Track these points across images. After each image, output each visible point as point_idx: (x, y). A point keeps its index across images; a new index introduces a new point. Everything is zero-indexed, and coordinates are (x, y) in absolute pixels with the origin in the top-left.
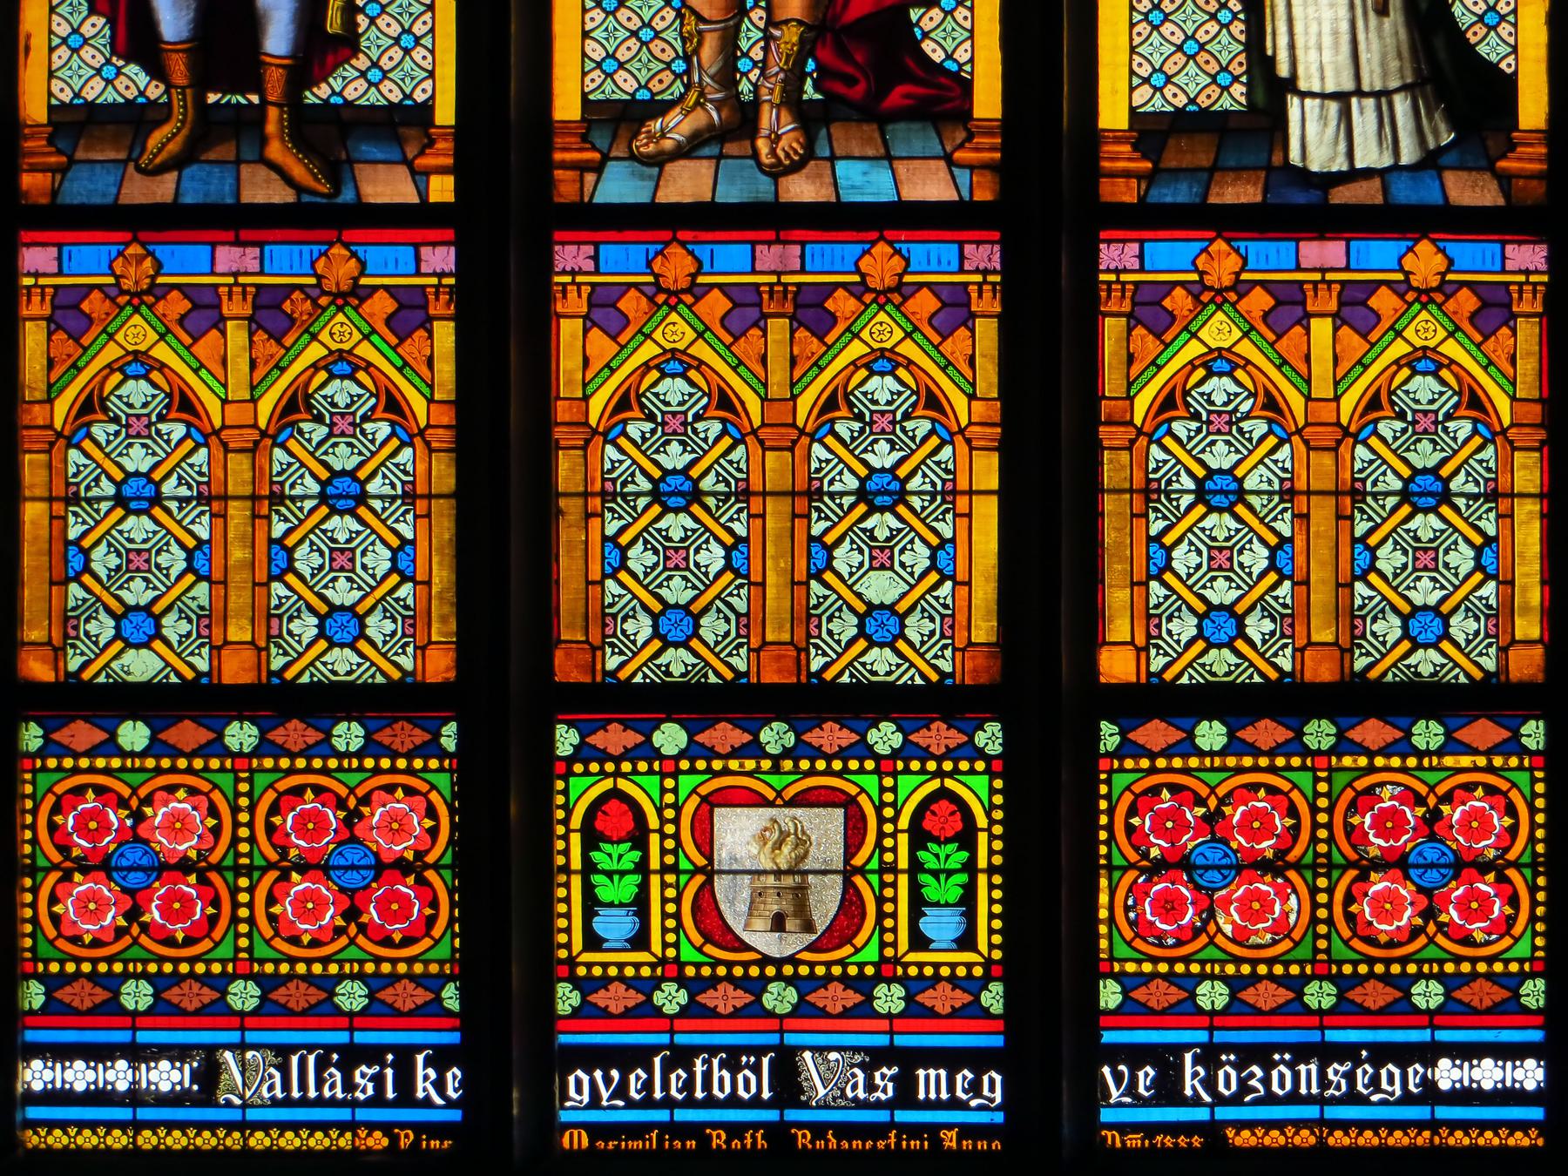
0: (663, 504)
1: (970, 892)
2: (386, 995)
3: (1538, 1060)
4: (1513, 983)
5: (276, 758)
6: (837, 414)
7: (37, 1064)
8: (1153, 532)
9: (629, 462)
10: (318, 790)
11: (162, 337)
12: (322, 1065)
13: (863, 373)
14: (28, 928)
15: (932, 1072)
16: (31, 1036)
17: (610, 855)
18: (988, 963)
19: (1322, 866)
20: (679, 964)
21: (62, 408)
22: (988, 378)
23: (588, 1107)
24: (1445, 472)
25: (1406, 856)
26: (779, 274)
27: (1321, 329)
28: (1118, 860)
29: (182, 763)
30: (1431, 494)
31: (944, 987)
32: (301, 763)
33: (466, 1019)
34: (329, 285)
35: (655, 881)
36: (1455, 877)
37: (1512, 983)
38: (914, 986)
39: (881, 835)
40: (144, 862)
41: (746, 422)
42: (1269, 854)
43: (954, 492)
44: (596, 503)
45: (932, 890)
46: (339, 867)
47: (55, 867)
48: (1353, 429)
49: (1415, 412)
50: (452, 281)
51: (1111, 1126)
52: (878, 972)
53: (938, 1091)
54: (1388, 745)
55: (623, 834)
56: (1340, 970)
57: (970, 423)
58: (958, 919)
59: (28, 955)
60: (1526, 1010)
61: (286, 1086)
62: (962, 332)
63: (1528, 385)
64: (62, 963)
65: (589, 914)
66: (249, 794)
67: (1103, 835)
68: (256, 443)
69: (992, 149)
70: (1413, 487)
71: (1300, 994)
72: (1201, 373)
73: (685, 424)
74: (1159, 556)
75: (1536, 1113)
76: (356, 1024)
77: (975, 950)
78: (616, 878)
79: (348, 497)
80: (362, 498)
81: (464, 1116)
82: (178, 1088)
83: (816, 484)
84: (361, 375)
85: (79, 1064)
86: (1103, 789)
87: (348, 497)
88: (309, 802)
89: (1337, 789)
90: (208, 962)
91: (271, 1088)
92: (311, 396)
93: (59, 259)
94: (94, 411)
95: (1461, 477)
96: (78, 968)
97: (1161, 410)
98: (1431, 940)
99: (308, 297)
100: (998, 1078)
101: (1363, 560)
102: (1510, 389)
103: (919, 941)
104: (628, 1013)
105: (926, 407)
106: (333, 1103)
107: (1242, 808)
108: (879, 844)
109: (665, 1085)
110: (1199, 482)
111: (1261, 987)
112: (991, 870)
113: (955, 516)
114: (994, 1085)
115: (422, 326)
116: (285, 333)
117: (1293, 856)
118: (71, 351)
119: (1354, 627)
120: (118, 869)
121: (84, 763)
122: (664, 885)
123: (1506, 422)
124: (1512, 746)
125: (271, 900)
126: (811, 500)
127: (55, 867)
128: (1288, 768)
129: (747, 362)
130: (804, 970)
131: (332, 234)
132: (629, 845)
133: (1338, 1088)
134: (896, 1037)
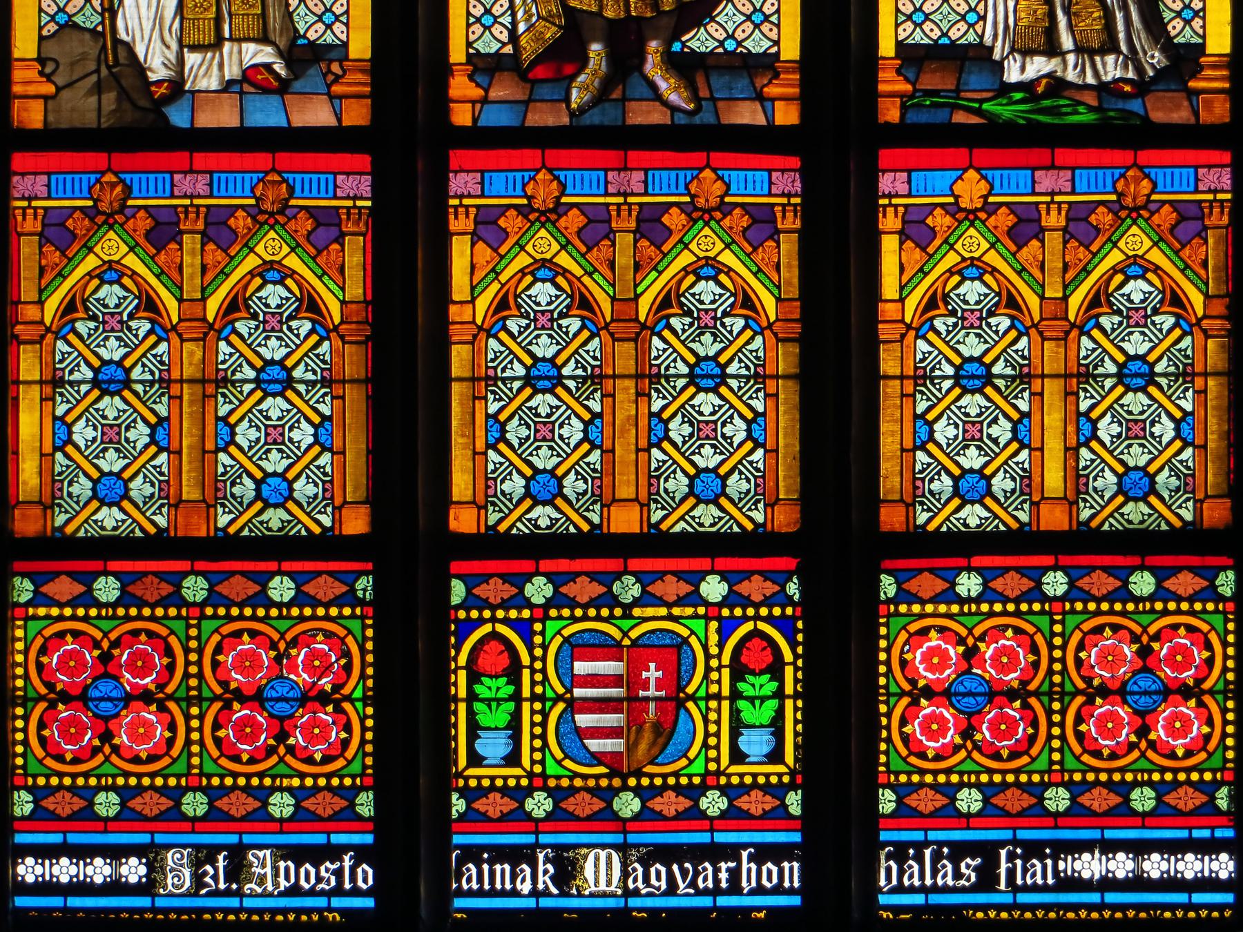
0: (533, 387)
1: (516, 716)
2: (1170, 799)
4: (1037, 791)
5: (909, 604)
6: (937, 312)
8: (919, 411)
9: (76, 354)
10: (253, 634)
11: (563, 247)
12: (937, 857)
13: (96, 282)
14: (19, 749)
15: (786, 865)
17: (753, 685)
18: (792, 773)
19: (1056, 693)
20: (544, 776)
21: (911, 303)
24: (987, 360)
25: (260, 690)
27: (625, 241)
28: (893, 689)
31: (670, 795)
32: (1105, 606)
33: (378, 823)
35: (526, 706)
36: (990, 702)
38: (902, 791)
39: (708, 669)
40: (114, 694)
41: (1028, 319)
42: (1015, 684)
43: (1194, 374)
46: (272, 699)
48: (54, 328)
49: (964, 310)
50: (798, 200)
51: (887, 908)
53: (503, 882)
55: (764, 666)
56: (1071, 777)
57: (1042, 319)
58: (504, 741)
60: (360, 818)
62: (1035, 243)
63: (355, 289)
64: (48, 777)
65: (735, 734)
66: (198, 638)
67: (882, 669)
68: (638, 334)
69: (792, 86)
70: (698, 371)
71: (178, 804)
73: (715, 318)
76: (540, 829)
77: (469, 766)
80: (127, 383)
81: (1235, 898)
82: (40, 879)
83: (222, 374)
84: (289, 282)
85: (64, 861)
86: (883, 631)
88: (246, 644)
90: (1201, 772)
91: (705, 879)
92: (87, 300)
94: (239, 310)
95: (1001, 363)
96: (1097, 777)
97: (659, 309)
98: (1143, 755)
99: (1110, 210)
100: (370, 872)
101: (923, 432)
102: (776, 292)
103: (738, 756)
105: (1006, 307)
106: (912, 890)
107: (326, 648)
108: (706, 676)
109: (353, 878)
110: (1121, 366)
112: (796, 695)
113: (333, 398)
115: (1036, 237)
117: (1032, 687)
118: (220, 259)
119: (915, 488)
120: (956, 694)
121: (929, 608)
122: (533, 712)
123: (772, 318)
124: (1036, 594)
125: (1079, 720)
126: (218, 387)
128: (1031, 612)
129: (330, 272)
132: (768, 676)
133: (968, 879)
134: (244, 836)
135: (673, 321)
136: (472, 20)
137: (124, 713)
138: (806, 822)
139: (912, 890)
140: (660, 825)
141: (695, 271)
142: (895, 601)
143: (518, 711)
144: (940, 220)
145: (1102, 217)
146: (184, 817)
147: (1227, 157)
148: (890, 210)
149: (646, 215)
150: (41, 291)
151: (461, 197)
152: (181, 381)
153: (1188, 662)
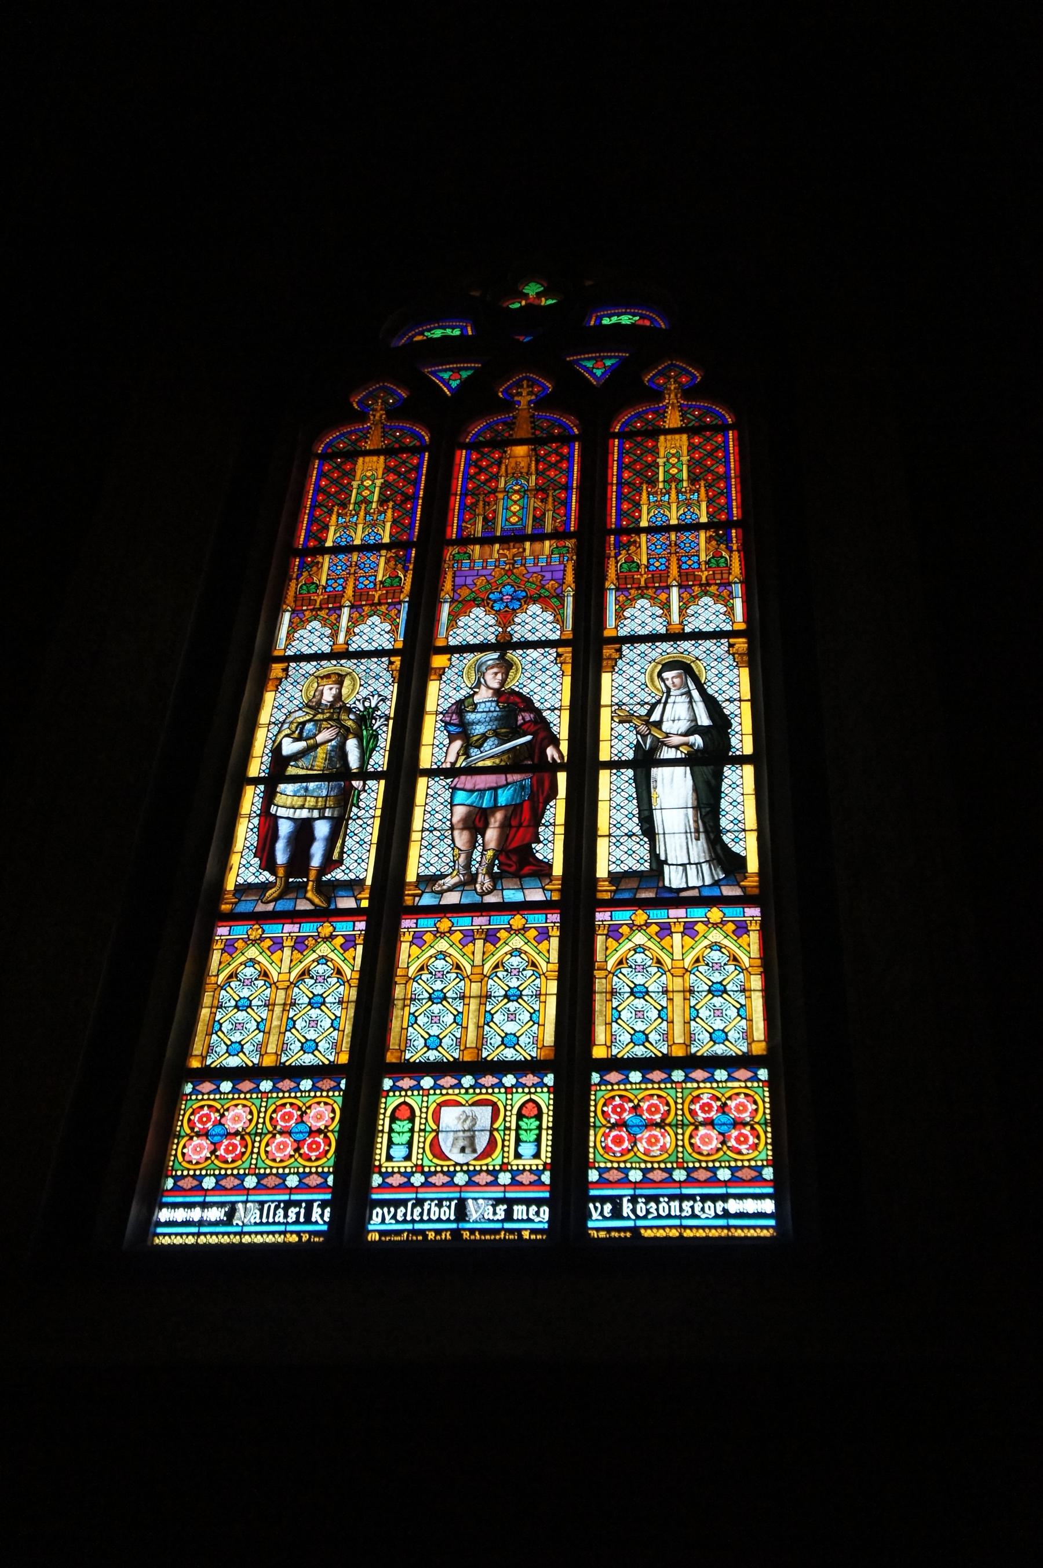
12: (277, 1208)
16: (593, 1192)
18: (545, 1164)
20: (422, 1166)
31: (484, 1174)
35: (416, 1135)
42: (659, 1121)
46: (719, 1125)
60: (765, 1180)
61: (261, 1217)
65: (389, 1147)
68: (607, 976)
81: (776, 1223)
89: (269, 1104)
101: (616, 1015)
103: (517, 1156)
104: (400, 1186)
105: (264, 976)
106: (279, 1223)
108: (504, 1120)
109: (429, 1213)
112: (548, 1128)
119: (691, 1037)
130: (471, 1168)
135: (623, 970)
136: (420, 865)
137: (209, 1142)
138: (553, 1186)
139: (279, 1223)
140: (523, 1188)
141: (635, 950)
142: (599, 1084)
143: (412, 1138)
144: (625, 930)
145: (311, 942)
146: (674, 1181)
147: (365, 918)
148: (407, 933)
149: (298, 940)
150: (606, 957)
151: (221, 936)
152: (470, 997)
153: (657, 1111)
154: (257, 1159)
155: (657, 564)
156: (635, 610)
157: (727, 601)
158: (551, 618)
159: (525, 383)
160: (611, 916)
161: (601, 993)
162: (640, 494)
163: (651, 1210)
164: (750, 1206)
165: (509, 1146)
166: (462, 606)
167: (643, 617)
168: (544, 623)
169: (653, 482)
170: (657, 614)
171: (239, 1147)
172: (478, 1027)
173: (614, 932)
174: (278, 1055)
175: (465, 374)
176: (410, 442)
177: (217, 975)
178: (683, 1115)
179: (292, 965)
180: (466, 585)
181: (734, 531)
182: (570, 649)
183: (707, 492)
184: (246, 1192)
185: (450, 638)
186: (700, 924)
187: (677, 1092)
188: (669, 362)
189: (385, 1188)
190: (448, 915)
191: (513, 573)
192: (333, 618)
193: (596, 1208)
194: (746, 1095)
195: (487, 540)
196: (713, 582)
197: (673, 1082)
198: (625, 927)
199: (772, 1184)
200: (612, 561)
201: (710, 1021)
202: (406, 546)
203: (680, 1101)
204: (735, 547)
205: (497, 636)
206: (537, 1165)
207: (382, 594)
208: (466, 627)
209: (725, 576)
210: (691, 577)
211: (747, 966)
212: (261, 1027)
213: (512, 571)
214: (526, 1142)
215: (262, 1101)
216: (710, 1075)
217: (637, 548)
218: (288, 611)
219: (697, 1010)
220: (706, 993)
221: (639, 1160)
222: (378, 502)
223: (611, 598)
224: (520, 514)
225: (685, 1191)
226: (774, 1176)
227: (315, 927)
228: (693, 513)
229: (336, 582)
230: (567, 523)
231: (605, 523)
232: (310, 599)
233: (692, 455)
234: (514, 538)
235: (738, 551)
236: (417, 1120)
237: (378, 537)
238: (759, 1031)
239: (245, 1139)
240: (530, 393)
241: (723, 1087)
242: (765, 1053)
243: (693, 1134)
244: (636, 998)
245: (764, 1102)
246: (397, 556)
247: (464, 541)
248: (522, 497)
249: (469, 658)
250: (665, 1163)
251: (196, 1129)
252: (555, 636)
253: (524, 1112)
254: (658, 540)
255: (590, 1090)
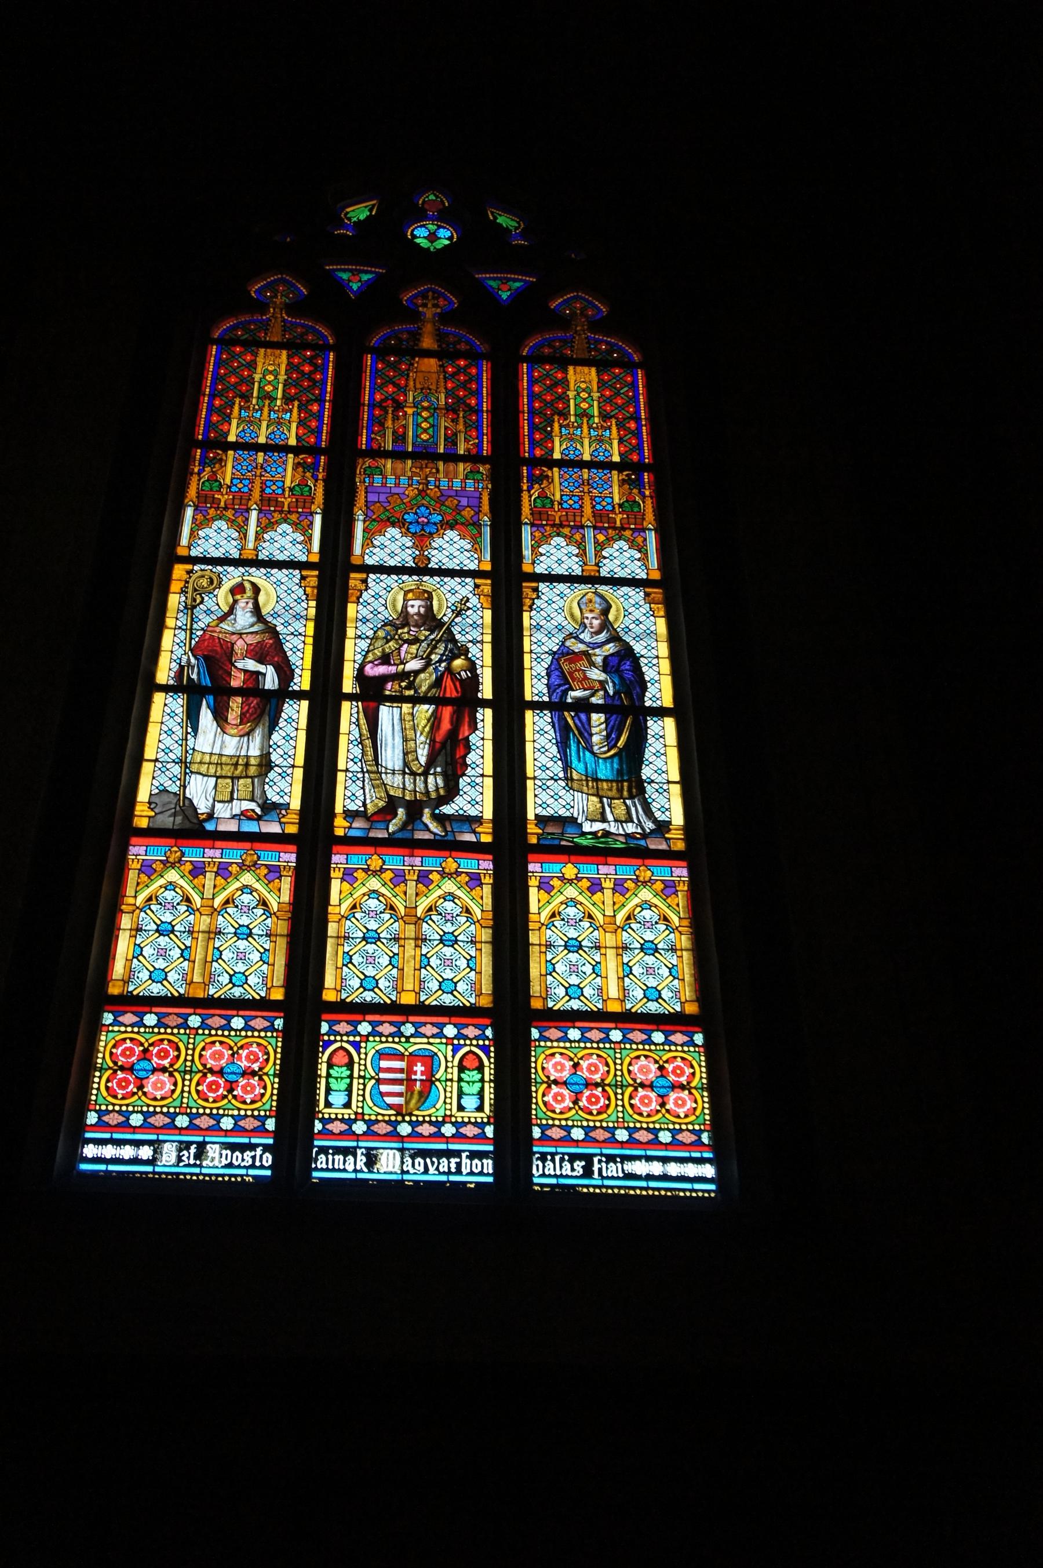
3: (711, 1165)
7: (91, 1146)
12: (562, 1160)
18: (489, 1117)
22: (488, 902)
23: (423, 1173)
26: (412, 866)
28: (539, 1080)
29: (256, 1034)
30: (451, 941)
33: (276, 1134)
34: (372, 868)
35: (355, 1082)
37: (263, 1119)
44: (212, 936)
45: (466, 1088)
46: (228, 1073)
47: (200, 1071)
52: (444, 1120)
54: (134, 1023)
59: (93, 1102)
60: (267, 1131)
65: (460, 1097)
72: (639, 909)
74: (217, 953)
75: (712, 1187)
78: (339, 1080)
79: (244, 934)
87: (244, 934)
89: (108, 1039)
93: (347, 859)
101: (425, 962)
103: (461, 1108)
104: (431, 1136)
105: (390, 909)
106: (550, 1176)
109: (261, 1160)
111: (158, 1116)
112: (491, 1081)
114: (488, 1165)
116: (152, 875)
119: (547, 991)
127: (200, 1071)
131: (447, 853)
138: (496, 1140)
139: (550, 1176)
154: (188, 1098)
155: (240, 486)
156: (551, 547)
157: (305, 530)
158: (410, 544)
159: (430, 294)
160: (422, 862)
161: (409, 939)
162: (552, 426)
163: (183, 1158)
164: (691, 1170)
165: (358, 1095)
166: (378, 524)
167: (393, 547)
168: (403, 548)
169: (564, 414)
170: (298, 540)
171: (258, 1088)
172: (337, 968)
173: (148, 869)
174: (205, 985)
175: (365, 277)
176: (242, 335)
177: (135, 897)
178: (622, 1075)
179: (138, 889)
180: (379, 502)
181: (646, 474)
182: (489, 582)
183: (300, 412)
184: (355, 1137)
185: (366, 557)
186: (435, 873)
187: (615, 1053)
188: (280, 276)
189: (457, 1138)
190: (454, 854)
191: (427, 495)
192: (240, 520)
193: (433, 1163)
194: (683, 1059)
195: (399, 455)
196: (567, 523)
197: (611, 1042)
198: (435, 873)
199: (272, 1135)
200: (195, 478)
201: (232, 963)
202: (314, 451)
203: (618, 1061)
204: (320, 477)
205: (414, 558)
206: (482, 1118)
207: (623, 518)
208: (440, 549)
209: (578, 519)
210: (273, 503)
211: (479, 918)
212: (186, 954)
213: (425, 491)
214: (469, 1095)
215: (189, 1038)
216: (563, 1034)
217: (550, 483)
218: (190, 506)
219: (631, 967)
220: (360, 940)
221: (667, 1121)
222: (282, 399)
223: (526, 532)
224: (420, 431)
225: (452, 1147)
226: (494, 1134)
227: (239, 854)
228: (606, 450)
229: (241, 482)
230: (479, 446)
231: (194, 434)
232: (214, 498)
233: (603, 393)
234: (425, 455)
235: (651, 497)
236: (356, 1066)
237: (283, 437)
238: (487, 987)
239: (263, 1080)
240: (435, 306)
241: (575, 1047)
242: (490, 1005)
243: (633, 1095)
244: (445, 945)
245: (700, 1066)
246: (305, 462)
247: (377, 453)
248: (432, 415)
249: (580, 588)
250: (693, 1125)
251: (120, 1063)
252: (473, 566)
253: (464, 1064)
254: (275, 461)
255: (530, 1047)
